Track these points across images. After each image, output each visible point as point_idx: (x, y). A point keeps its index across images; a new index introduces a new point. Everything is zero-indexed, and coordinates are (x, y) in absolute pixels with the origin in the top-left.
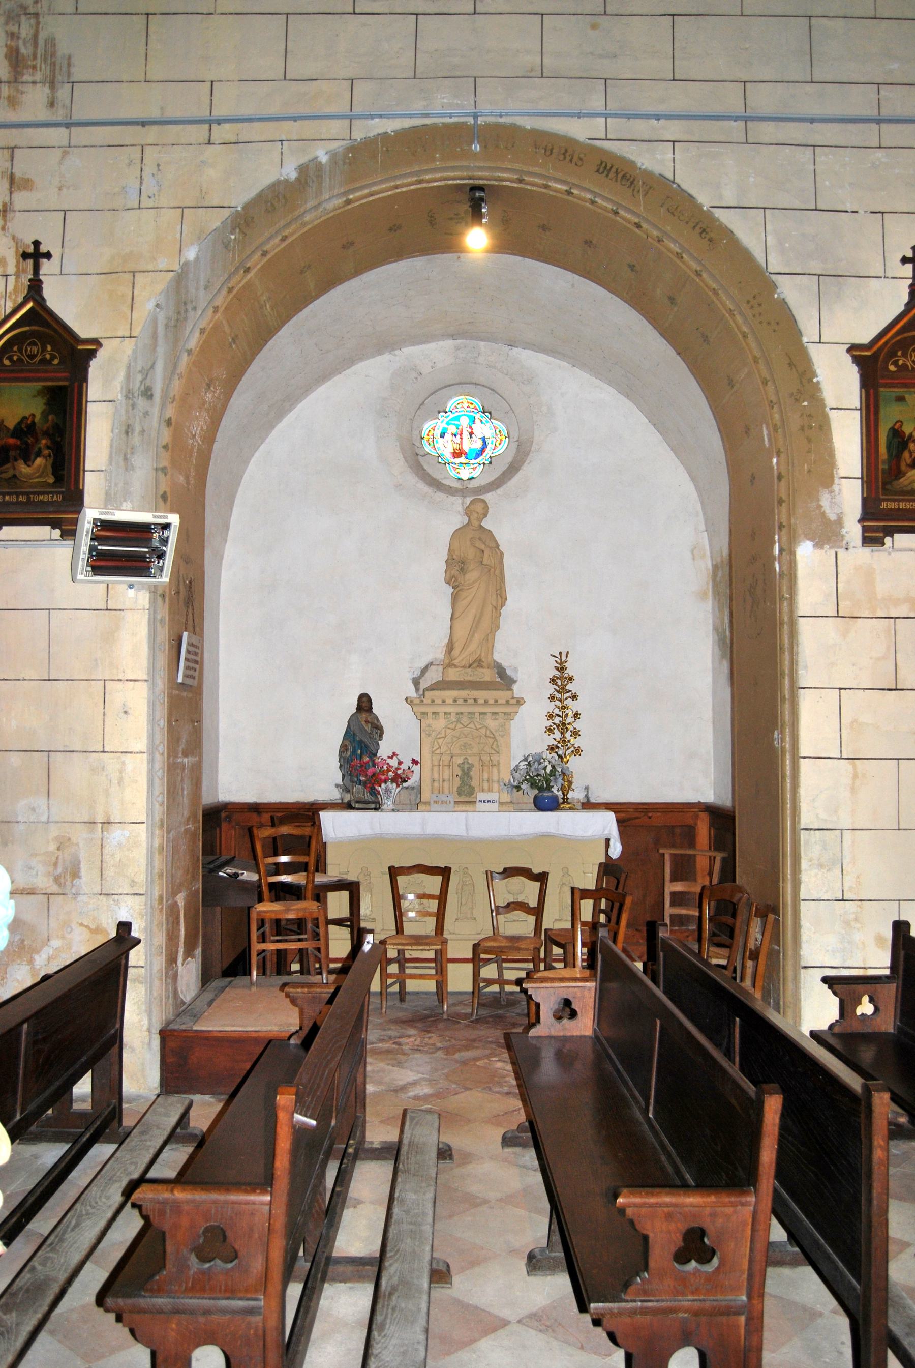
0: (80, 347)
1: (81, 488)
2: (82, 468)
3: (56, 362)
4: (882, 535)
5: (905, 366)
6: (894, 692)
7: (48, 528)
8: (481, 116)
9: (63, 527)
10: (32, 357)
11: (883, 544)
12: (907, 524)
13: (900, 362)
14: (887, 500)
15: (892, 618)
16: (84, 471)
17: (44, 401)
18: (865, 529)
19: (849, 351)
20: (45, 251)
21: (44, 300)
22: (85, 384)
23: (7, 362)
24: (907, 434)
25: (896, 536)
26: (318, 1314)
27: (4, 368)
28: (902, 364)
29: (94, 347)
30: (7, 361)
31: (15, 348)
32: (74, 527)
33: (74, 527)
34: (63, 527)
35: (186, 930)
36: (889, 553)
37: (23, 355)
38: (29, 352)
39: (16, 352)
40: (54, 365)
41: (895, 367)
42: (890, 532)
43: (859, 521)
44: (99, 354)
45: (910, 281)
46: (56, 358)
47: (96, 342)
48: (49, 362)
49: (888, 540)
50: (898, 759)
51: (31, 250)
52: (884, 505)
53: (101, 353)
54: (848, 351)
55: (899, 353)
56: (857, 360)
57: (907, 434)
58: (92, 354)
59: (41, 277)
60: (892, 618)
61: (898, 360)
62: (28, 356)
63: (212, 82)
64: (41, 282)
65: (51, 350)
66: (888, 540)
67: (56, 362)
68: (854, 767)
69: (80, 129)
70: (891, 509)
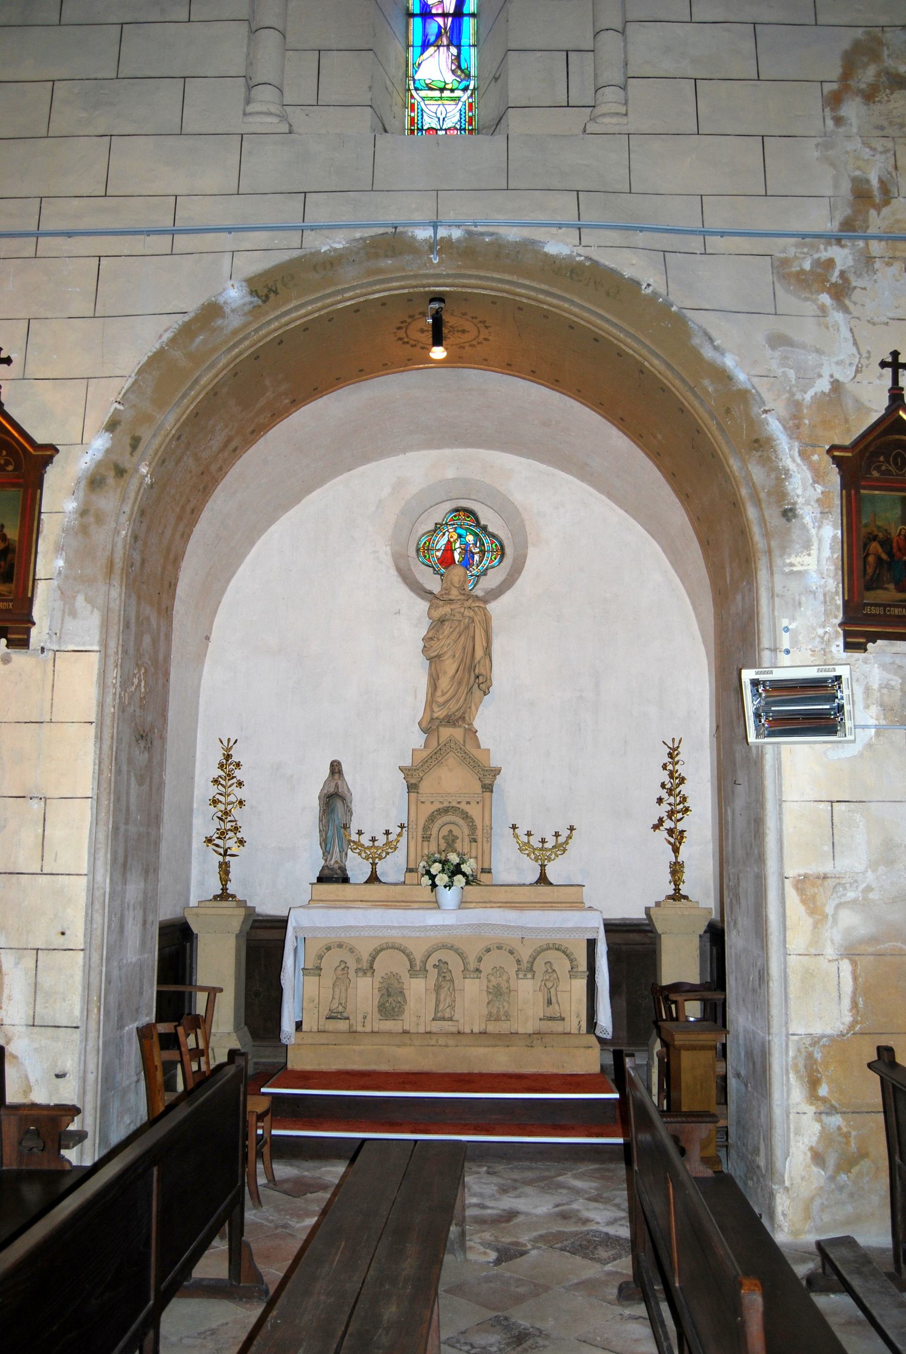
3: (10, 468)
8: (441, 225)
9: (9, 636)
11: (866, 650)
12: (891, 630)
17: (814, 1145)
18: (846, 634)
20: (6, 356)
27: (883, 1075)
29: (49, 453)
35: (158, 1205)
39: (883, 462)
42: (873, 637)
47: (52, 449)
49: (870, 646)
54: (829, 452)
56: (837, 461)
58: (48, 460)
63: (176, 196)
65: (6, 456)
66: (870, 646)
69: (48, 239)
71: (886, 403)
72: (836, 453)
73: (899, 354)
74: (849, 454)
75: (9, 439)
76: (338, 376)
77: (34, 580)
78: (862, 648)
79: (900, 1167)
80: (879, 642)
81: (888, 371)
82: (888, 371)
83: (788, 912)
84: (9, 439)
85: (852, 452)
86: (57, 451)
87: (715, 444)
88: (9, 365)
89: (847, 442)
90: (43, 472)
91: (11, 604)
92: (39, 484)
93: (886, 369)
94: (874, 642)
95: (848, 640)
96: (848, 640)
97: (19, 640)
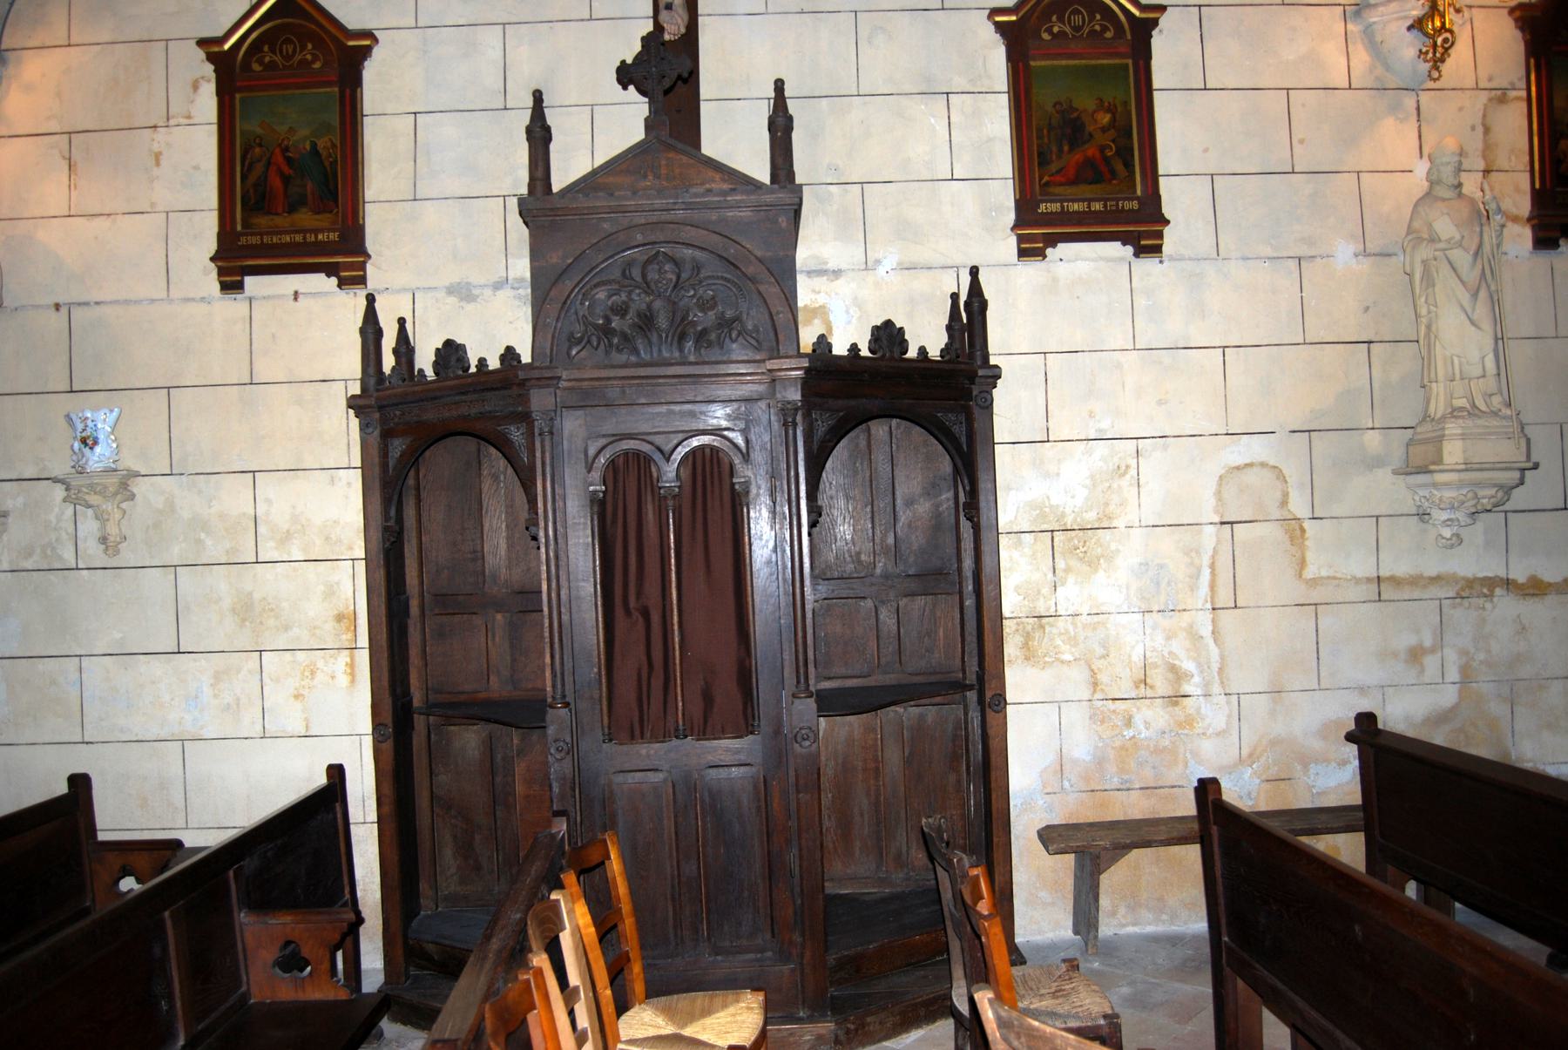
0: (351, 43)
1: (361, 222)
2: (361, 200)
4: (1041, 245)
7: (1118, 244)
9: (342, 274)
10: (1077, 29)
11: (1045, 257)
13: (1056, 30)
14: (1046, 201)
16: (1014, 178)
18: (1021, 239)
19: (990, 17)
23: (1046, 36)
26: (1070, 882)
28: (270, 62)
29: (367, 43)
32: (1158, 242)
33: (1159, 242)
34: (342, 274)
40: (1106, 39)
41: (260, 65)
42: (1052, 241)
43: (212, 259)
44: (375, 51)
48: (309, 63)
49: (1049, 251)
52: (1043, 208)
53: (377, 52)
55: (1054, 18)
56: (1000, 27)
58: (366, 52)
61: (1052, 27)
66: (1049, 251)
72: (998, 19)
74: (1014, 18)
76: (163, 162)
77: (364, 202)
78: (1041, 254)
79: (1229, 949)
80: (1060, 245)
83: (636, 483)
86: (376, 40)
92: (357, 82)
95: (362, 273)
96: (362, 273)
97: (233, 282)
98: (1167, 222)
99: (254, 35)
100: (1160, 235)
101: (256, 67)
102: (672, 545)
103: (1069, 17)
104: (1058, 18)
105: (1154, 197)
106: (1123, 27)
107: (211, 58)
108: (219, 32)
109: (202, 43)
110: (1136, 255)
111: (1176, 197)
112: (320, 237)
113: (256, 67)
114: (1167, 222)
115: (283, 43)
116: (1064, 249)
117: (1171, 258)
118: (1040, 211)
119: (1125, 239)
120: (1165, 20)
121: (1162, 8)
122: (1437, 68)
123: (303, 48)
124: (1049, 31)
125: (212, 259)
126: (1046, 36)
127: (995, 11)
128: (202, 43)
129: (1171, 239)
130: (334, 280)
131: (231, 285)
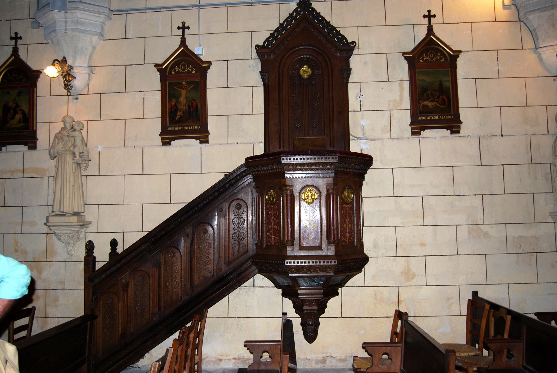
1: (35, 129)
5: (179, 71)
6: (4, 208)
10: (184, 70)
13: (425, 59)
14: (421, 116)
15: (4, 178)
21: (19, 56)
22: (35, 89)
24: (10, 106)
25: (8, 146)
28: (426, 59)
30: (173, 72)
31: (424, 55)
32: (459, 129)
33: (459, 129)
36: (5, 153)
37: (180, 69)
38: (431, 56)
41: (422, 61)
42: (423, 129)
43: (160, 135)
45: (428, 25)
46: (194, 70)
49: (422, 132)
50: (3, 234)
51: (19, 36)
52: (420, 118)
53: (211, 67)
55: (176, 67)
56: (406, 58)
57: (10, 106)
58: (208, 68)
59: (18, 46)
60: (4, 178)
62: (182, 70)
64: (185, 39)
65: (192, 67)
66: (422, 132)
67: (194, 72)
68: (15, 236)
70: (171, 130)
71: (426, 32)
73: (431, 11)
74: (452, 53)
75: (170, 65)
81: (427, 19)
82: (427, 19)
84: (170, 65)
85: (412, 55)
87: (524, 357)
88: (21, 40)
89: (410, 50)
90: (36, 81)
91: (28, 133)
93: (426, 18)
94: (424, 131)
98: (462, 123)
99: (171, 64)
100: (459, 127)
101: (173, 73)
102: (339, 232)
103: (181, 67)
104: (178, 67)
105: (457, 116)
106: (447, 57)
107: (158, 70)
108: (161, 61)
109: (156, 66)
110: (452, 133)
111: (212, 124)
112: (176, 128)
113: (173, 73)
114: (462, 123)
115: (182, 65)
116: (177, 141)
117: (38, 150)
118: (419, 119)
119: (447, 128)
120: (461, 55)
121: (460, 52)
122: (69, 92)
123: (437, 55)
124: (422, 59)
125: (160, 135)
126: (421, 61)
127: (404, 54)
128: (156, 66)
129: (464, 129)
130: (198, 141)
131: (166, 142)
